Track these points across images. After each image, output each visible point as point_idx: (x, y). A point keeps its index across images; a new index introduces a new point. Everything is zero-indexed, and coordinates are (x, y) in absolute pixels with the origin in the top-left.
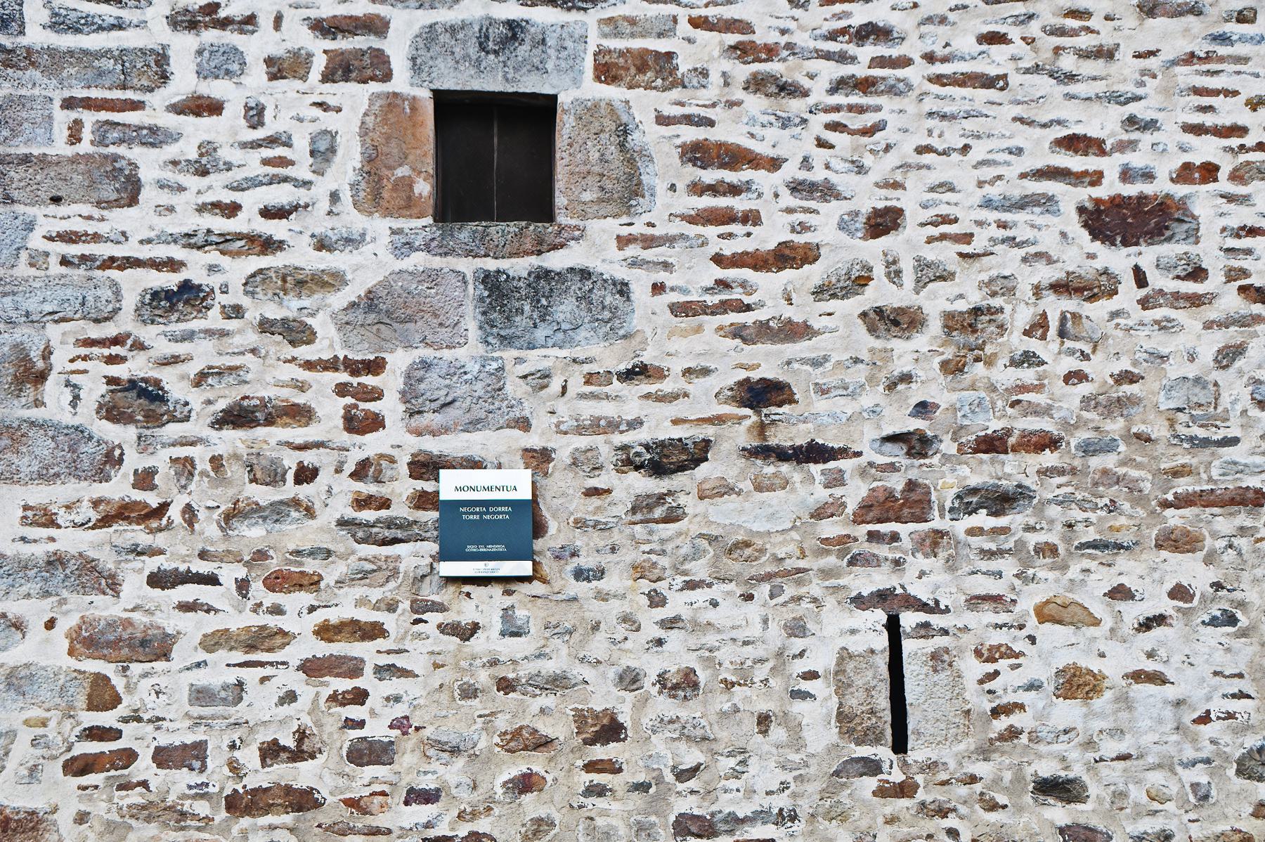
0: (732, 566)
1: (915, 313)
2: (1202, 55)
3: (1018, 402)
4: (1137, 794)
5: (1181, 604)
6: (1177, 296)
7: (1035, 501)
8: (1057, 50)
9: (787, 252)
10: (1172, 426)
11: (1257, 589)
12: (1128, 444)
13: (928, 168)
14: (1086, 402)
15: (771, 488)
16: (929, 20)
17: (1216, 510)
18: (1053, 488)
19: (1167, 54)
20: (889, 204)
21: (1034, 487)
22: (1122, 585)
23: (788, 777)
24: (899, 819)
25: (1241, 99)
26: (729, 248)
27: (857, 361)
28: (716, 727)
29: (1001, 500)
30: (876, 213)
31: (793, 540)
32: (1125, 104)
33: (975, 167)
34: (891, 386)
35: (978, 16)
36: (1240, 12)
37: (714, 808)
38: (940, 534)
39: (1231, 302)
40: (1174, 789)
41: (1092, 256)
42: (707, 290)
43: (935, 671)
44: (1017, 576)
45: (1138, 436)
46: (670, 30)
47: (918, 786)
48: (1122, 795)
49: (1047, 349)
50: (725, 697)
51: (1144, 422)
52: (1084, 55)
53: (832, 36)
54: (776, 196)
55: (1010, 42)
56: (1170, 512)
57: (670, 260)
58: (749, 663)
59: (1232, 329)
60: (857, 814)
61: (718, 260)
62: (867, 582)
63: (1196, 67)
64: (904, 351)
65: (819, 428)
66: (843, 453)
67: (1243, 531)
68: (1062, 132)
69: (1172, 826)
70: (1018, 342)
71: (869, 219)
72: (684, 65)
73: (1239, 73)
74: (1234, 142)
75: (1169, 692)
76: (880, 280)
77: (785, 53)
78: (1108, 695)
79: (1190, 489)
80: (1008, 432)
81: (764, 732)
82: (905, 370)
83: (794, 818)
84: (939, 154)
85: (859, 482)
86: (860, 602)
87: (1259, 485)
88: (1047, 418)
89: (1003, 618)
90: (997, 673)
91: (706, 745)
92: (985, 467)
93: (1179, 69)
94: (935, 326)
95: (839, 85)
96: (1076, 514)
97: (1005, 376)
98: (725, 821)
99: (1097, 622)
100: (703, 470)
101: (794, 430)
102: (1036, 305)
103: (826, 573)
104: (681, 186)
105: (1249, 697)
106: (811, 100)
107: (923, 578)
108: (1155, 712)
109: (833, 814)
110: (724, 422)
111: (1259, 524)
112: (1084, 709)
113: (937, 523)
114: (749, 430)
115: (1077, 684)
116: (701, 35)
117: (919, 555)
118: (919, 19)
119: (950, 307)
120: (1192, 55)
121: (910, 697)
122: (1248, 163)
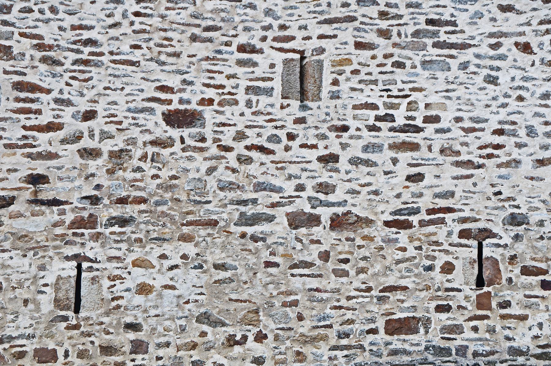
0: (20, 244)
1: (98, 151)
2: (212, 58)
3: (134, 185)
4: (160, 329)
5: (184, 261)
6: (195, 147)
7: (136, 222)
8: (160, 53)
9: (51, 126)
10: (188, 196)
11: (211, 256)
12: (172, 202)
13: (108, 95)
14: (159, 186)
15: (37, 215)
16: (112, 38)
17: (200, 227)
18: (144, 217)
19: (199, 57)
20: (92, 108)
21: (136, 217)
22: (164, 254)
23: (33, 322)
24: (73, 337)
25: (224, 75)
26: (28, 123)
27: (75, 168)
28: (7, 304)
29: (123, 222)
30: (87, 112)
31: (44, 235)
32: (183, 74)
33: (126, 96)
34: (87, 178)
35: (131, 38)
36: (226, 42)
37: (3, 333)
38: (99, 234)
39: (214, 151)
40: (173, 327)
41: (166, 132)
42: (19, 139)
43: (93, 284)
44: (126, 250)
45: (176, 199)
46: (10, 37)
47: (81, 326)
48: (154, 329)
49: (145, 166)
50: (12, 293)
51: (178, 194)
52: (169, 55)
53: (75, 43)
54: (49, 104)
55: (142, 48)
56: (184, 227)
57: (5, 127)
58: (23, 280)
59: (213, 161)
60: (58, 336)
61: (24, 127)
62: (70, 251)
63: (209, 62)
64: (93, 165)
65: (58, 193)
66: (66, 203)
67: (209, 235)
68: (158, 84)
69: (171, 340)
70: (135, 162)
71: (83, 114)
72: (15, 51)
73: (224, 65)
74: (220, 91)
75: (176, 292)
76: (86, 137)
77: (56, 48)
78: (154, 293)
79: (192, 219)
80: (129, 196)
81: (26, 306)
82: (93, 172)
83: (33, 337)
84: (112, 90)
85: (71, 213)
86: (68, 258)
87: (216, 219)
88: (143, 192)
89: (120, 265)
90: (115, 285)
91: (3, 310)
92: (119, 209)
93: (203, 62)
94: (106, 156)
95: (75, 62)
96: (151, 227)
97: (130, 175)
98: (7, 338)
99: (154, 267)
100: (12, 208)
101: (48, 193)
102: (144, 149)
103: (55, 247)
104: (11, 99)
105: (204, 294)
106: (65, 67)
107: (92, 249)
108: (170, 300)
109: (49, 336)
110: (21, 190)
111: (215, 233)
112: (145, 299)
113: (99, 230)
114: (31, 193)
115: (144, 289)
116: (23, 40)
117: (91, 241)
118: (108, 38)
119: (111, 149)
120: (208, 57)
121: (82, 294)
122: (224, 99)
